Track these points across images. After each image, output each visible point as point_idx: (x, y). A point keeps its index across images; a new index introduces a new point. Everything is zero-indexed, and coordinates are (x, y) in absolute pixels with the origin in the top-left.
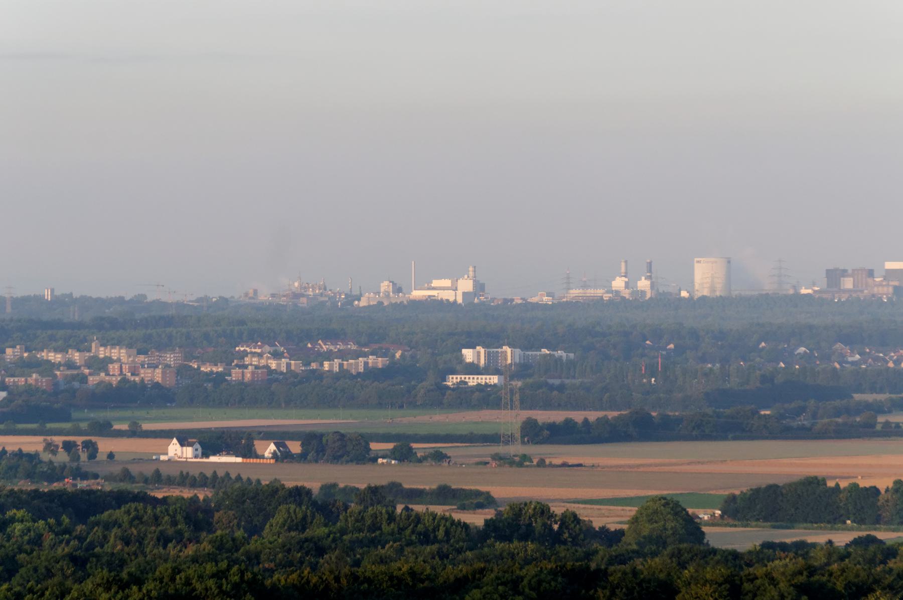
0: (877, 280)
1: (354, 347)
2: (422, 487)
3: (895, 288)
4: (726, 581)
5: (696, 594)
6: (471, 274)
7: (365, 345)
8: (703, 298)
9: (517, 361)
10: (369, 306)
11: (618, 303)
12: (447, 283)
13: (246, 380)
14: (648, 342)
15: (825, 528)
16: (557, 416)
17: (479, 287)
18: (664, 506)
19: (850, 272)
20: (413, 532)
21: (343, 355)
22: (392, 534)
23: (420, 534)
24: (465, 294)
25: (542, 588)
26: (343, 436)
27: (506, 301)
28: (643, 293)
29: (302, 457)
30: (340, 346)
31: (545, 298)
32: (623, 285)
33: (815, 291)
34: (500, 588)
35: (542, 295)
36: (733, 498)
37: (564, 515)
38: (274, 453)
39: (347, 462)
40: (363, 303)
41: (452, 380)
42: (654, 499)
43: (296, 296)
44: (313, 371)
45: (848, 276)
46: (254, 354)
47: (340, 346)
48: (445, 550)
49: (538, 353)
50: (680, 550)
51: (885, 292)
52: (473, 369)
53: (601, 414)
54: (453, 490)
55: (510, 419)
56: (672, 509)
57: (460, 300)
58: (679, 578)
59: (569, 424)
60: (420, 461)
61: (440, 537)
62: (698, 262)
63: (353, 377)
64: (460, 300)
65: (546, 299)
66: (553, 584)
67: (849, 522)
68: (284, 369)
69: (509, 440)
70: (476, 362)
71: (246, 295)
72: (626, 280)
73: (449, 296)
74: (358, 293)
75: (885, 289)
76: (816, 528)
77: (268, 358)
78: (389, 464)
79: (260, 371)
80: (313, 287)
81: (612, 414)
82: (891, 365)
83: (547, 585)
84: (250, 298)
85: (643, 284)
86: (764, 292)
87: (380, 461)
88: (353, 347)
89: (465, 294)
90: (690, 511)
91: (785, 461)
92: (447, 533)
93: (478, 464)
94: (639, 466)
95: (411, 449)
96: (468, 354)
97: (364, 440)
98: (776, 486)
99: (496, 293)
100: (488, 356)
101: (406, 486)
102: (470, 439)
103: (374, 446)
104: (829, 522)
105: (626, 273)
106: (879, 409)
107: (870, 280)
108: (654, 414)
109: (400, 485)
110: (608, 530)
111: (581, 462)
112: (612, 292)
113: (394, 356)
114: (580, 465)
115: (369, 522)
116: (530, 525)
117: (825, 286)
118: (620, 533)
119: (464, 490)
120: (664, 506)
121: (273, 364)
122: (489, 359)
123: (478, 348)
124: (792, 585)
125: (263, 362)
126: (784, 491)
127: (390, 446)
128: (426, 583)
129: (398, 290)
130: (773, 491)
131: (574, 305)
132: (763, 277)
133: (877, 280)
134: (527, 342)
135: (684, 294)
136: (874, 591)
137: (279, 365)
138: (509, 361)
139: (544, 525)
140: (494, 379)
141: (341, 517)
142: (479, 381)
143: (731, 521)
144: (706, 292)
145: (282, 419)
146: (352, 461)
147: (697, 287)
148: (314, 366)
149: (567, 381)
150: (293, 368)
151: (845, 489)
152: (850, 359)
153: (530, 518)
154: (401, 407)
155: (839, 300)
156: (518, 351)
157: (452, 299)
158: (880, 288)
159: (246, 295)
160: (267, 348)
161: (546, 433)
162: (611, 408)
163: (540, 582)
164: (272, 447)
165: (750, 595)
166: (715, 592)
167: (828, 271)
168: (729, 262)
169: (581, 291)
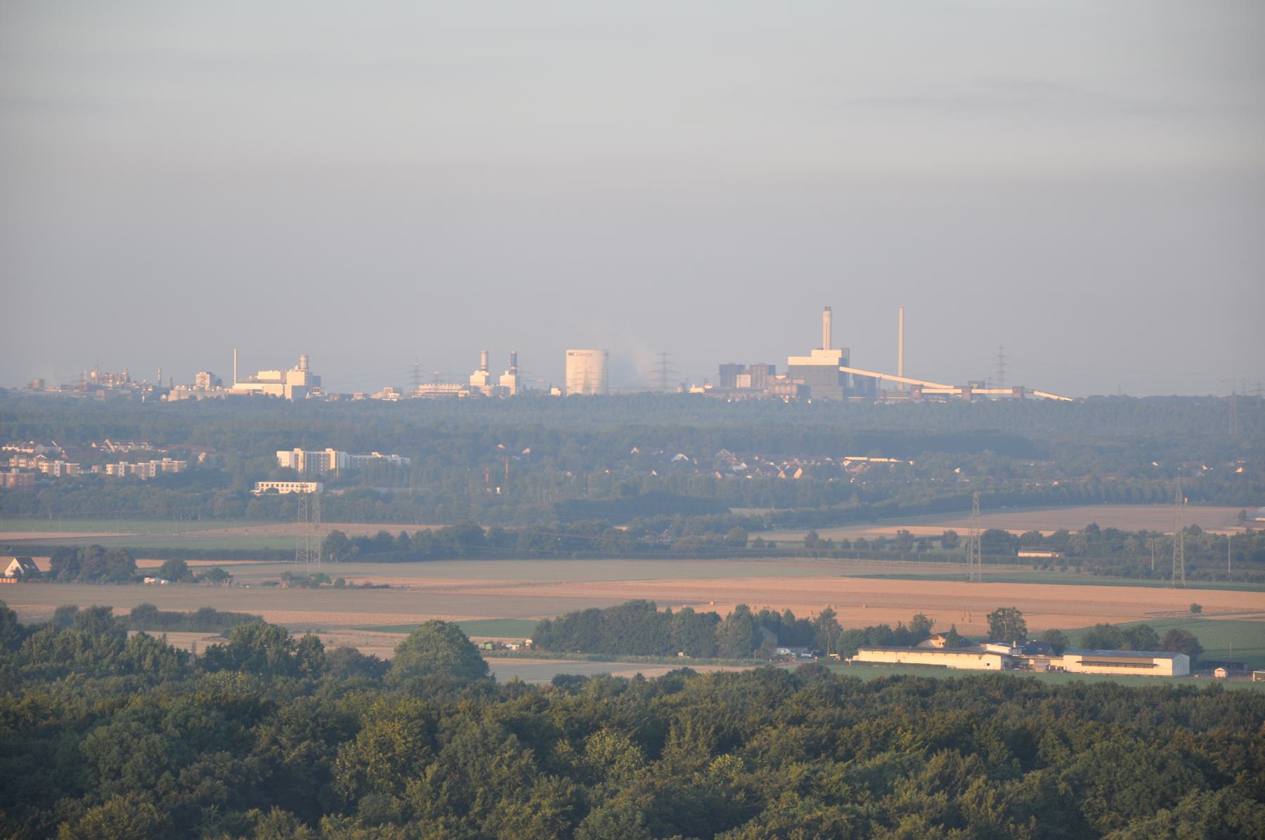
0: (779, 377)
1: (149, 448)
2: (180, 611)
3: (799, 386)
4: (421, 716)
5: (381, 730)
6: (303, 365)
7: (162, 446)
8: (576, 397)
9: (343, 465)
10: (180, 401)
11: (476, 400)
12: (276, 375)
13: (9, 485)
15: (652, 661)
16: (370, 530)
17: (313, 381)
18: (438, 631)
19: (747, 367)
20: (113, 661)
21: (132, 457)
22: (86, 663)
23: (122, 663)
24: (295, 388)
25: (189, 725)
26: (102, 551)
27: (343, 396)
28: (507, 389)
29: (52, 576)
30: (132, 447)
31: (391, 395)
33: (706, 390)
34: (134, 725)
35: (388, 391)
36: (547, 625)
37: (304, 641)
38: (17, 572)
39: (106, 582)
40: (173, 397)
41: (263, 486)
42: (428, 624)
43: (92, 388)
44: (94, 476)
46: (21, 455)
47: (132, 447)
48: (134, 683)
50: (422, 682)
51: (787, 392)
52: (289, 475)
53: (423, 528)
54: (218, 614)
55: (312, 533)
56: (447, 635)
57: (289, 396)
58: (365, 712)
59: (384, 540)
60: (195, 581)
61: (146, 667)
63: (140, 482)
64: (289, 396)
65: (393, 396)
66: (204, 719)
67: (681, 654)
68: (57, 473)
69: (308, 556)
71: (31, 386)
73: (276, 390)
74: (168, 385)
76: (642, 661)
77: (40, 459)
78: (157, 584)
79: (26, 475)
80: (114, 379)
81: (434, 528)
83: (196, 721)
84: (36, 390)
85: (507, 380)
87: (147, 580)
88: (146, 447)
89: (295, 388)
90: (472, 639)
91: (631, 583)
92: (156, 662)
93: (265, 584)
94: (455, 588)
95: (185, 566)
96: (285, 458)
97: (130, 555)
98: (597, 611)
99: (331, 388)
100: (308, 460)
101: (161, 609)
102: (265, 555)
103: (141, 564)
104: (658, 654)
105: (487, 366)
106: (756, 525)
107: (771, 378)
108: (486, 528)
109: (154, 608)
110: (377, 660)
111: (389, 583)
112: (469, 388)
113: (197, 459)
114: (386, 587)
115: (59, 649)
116: (262, 652)
117: (718, 385)
118: (388, 664)
119: (231, 614)
120: (438, 631)
121: (44, 467)
122: (309, 466)
124: (499, 721)
125: (33, 464)
126: (606, 617)
127: (159, 563)
128: (51, 720)
129: (216, 382)
130: (593, 616)
131: (425, 402)
132: (645, 369)
133: (779, 377)
134: (355, 444)
135: (555, 391)
136: (599, 728)
137: (51, 468)
138: (333, 466)
139: (278, 652)
140: (312, 487)
141: (24, 643)
142: (294, 489)
143: (543, 653)
144: (579, 390)
145: (1139, 676)
146: (112, 580)
147: (569, 383)
148: (95, 469)
149: (396, 490)
150: (68, 471)
151: (677, 615)
152: (735, 468)
153: (262, 644)
154: (195, 518)
155: (733, 401)
156: (343, 454)
157: (279, 394)
159: (31, 386)
160: (41, 448)
161: (355, 549)
162: (434, 522)
163: (187, 718)
164: (15, 564)
165: (448, 732)
166: (404, 729)
167: (722, 367)
168: (607, 355)
169: (433, 386)
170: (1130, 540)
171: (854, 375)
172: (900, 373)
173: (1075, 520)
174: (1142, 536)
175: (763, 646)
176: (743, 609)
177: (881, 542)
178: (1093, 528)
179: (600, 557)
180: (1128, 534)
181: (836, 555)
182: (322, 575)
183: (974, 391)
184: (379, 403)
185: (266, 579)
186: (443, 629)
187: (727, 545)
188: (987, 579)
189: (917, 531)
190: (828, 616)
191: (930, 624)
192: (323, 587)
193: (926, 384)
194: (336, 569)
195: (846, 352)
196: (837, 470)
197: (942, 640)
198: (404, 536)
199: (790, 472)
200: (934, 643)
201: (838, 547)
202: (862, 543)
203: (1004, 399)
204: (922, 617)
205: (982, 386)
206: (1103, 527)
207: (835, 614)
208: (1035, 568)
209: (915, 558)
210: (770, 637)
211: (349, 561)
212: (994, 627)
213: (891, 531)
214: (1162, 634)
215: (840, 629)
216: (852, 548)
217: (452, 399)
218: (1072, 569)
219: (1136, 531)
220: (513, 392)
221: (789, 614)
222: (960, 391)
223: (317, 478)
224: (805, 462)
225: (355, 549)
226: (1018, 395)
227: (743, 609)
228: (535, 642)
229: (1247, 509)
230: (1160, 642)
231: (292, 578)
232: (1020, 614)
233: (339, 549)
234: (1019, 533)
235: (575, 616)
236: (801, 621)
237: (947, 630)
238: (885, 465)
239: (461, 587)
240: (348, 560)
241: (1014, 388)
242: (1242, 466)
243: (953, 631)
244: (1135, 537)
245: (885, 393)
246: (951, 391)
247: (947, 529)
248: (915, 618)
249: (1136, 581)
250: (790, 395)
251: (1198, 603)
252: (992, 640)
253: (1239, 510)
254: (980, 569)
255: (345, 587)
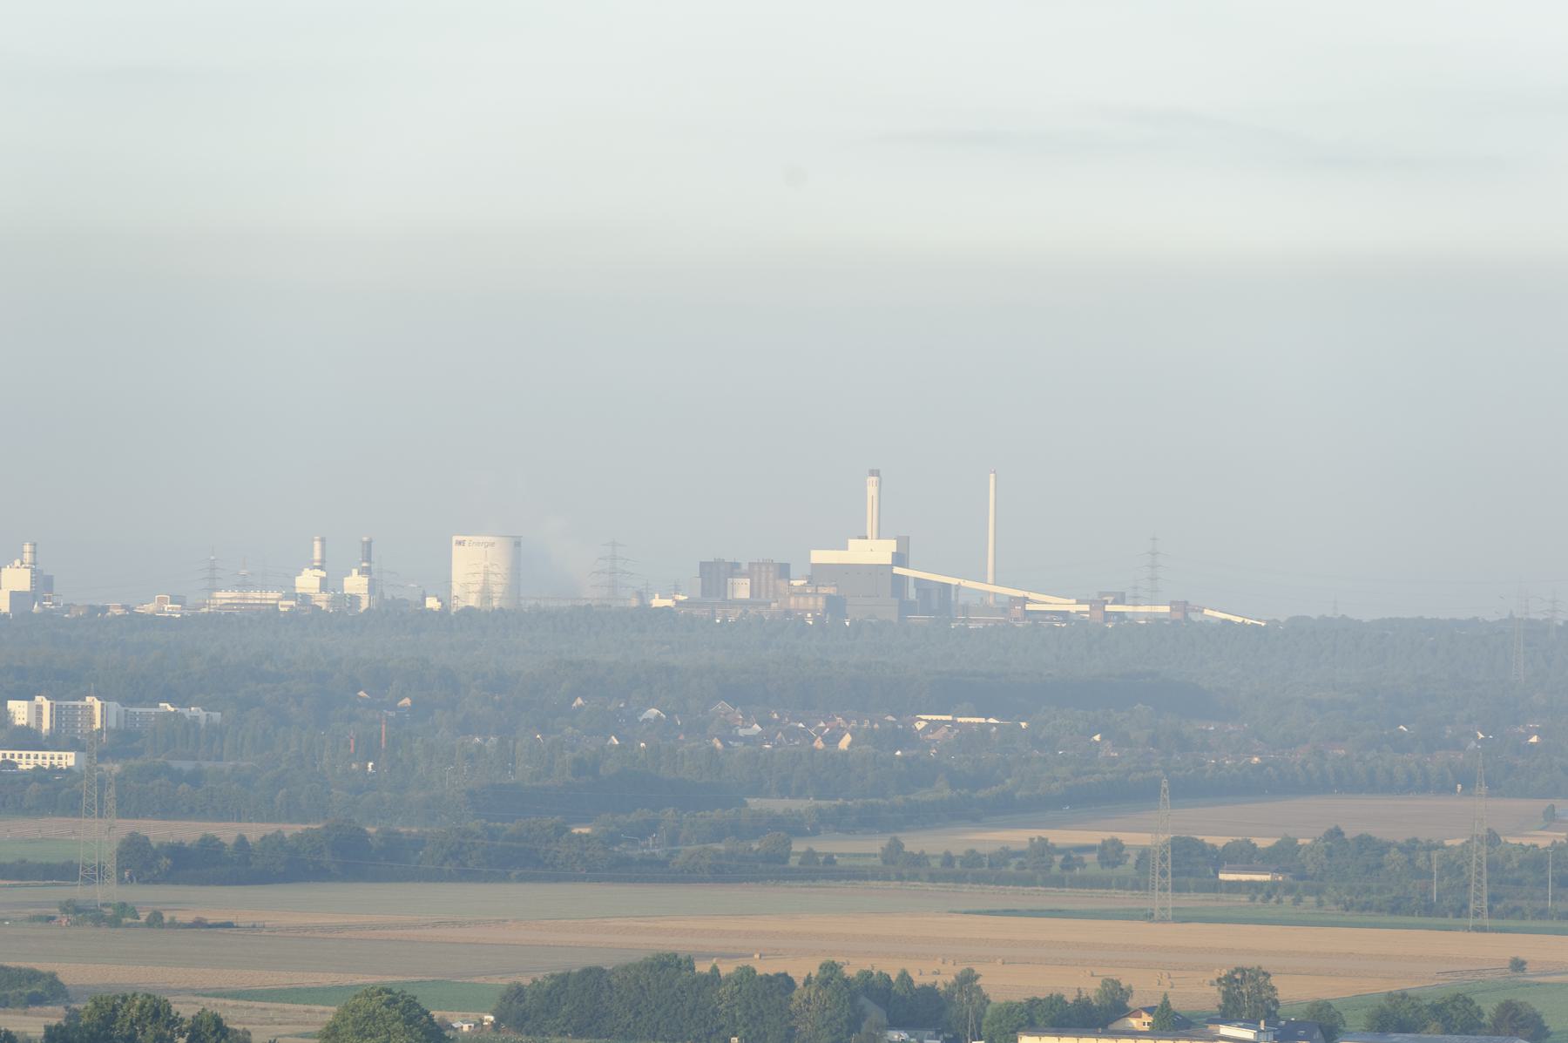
0: (796, 583)
3: (828, 598)
6: (27, 557)
8: (468, 611)
9: (113, 724)
11: (305, 616)
14: (362, 693)
16: (188, 832)
17: (43, 583)
19: (745, 567)
27: (93, 610)
28: (355, 599)
32: (317, 583)
33: (678, 603)
35: (162, 601)
36: (518, 992)
37: (197, 1021)
42: (369, 993)
45: (743, 575)
49: (153, 710)
51: (810, 606)
52: (28, 739)
53: (270, 828)
55: (96, 836)
62: (459, 543)
69: (94, 874)
70: (33, 725)
72: (323, 574)
75: (811, 601)
81: (291, 829)
82: (819, 744)
85: (355, 584)
86: (583, 603)
90: (437, 1015)
93: (33, 919)
96: (19, 711)
100: (57, 713)
105: (323, 561)
106: (794, 827)
107: (782, 584)
108: (371, 830)
111: (231, 919)
112: (294, 596)
114: (229, 925)
117: (698, 594)
120: (387, 1005)
122: (59, 724)
123: (38, 698)
126: (615, 981)
131: (223, 620)
133: (796, 583)
135: (432, 603)
140: (68, 759)
142: (40, 761)
144: (473, 601)
147: (456, 590)
149: (206, 765)
151: (729, 978)
152: (742, 732)
153: (132, 1024)
155: (724, 620)
156: (114, 706)
158: (801, 600)
167: (703, 565)
168: (518, 544)
169: (236, 594)
170: (1393, 853)
171: (916, 579)
172: (990, 578)
173: (1304, 820)
174: (1411, 847)
175: (865, 1027)
176: (831, 968)
177: (1005, 855)
178: (1336, 834)
179: (558, 879)
180: (1390, 845)
181: (933, 878)
182: (124, 905)
183: (1109, 608)
184: (151, 621)
185: (33, 911)
186: (395, 1001)
187: (762, 861)
188: (1182, 917)
189: (1061, 837)
190: (967, 980)
191: (1128, 993)
192: (128, 926)
193: (1032, 596)
194: (145, 896)
195: (903, 542)
196: (907, 737)
197: (1147, 1018)
198: (242, 842)
199: (833, 739)
200: (1134, 1023)
201: (936, 864)
202: (973, 859)
203: (1157, 621)
204: (1117, 983)
205: (1120, 599)
206: (1350, 833)
207: (977, 977)
208: (1253, 899)
209: (1059, 882)
210: (875, 1014)
211: (156, 882)
212: (1227, 997)
213: (1018, 837)
214: (1489, 1007)
215: (986, 1001)
216: (957, 865)
217: (269, 615)
218: (1310, 900)
219: (1401, 840)
220: (364, 605)
221: (905, 977)
222: (1086, 608)
223: (73, 745)
224: (854, 723)
225: (165, 862)
226: (1178, 615)
227: (831, 968)
228: (500, 1019)
229: (1557, 802)
230: (1486, 1019)
231: (77, 910)
232: (1267, 975)
233: (141, 862)
234: (1220, 841)
235: (564, 979)
236: (924, 987)
237: (1157, 1002)
238: (984, 728)
239: (346, 927)
240: (154, 881)
241: (1171, 604)
242: (1538, 732)
243: (1166, 1004)
244: (1401, 848)
245: (966, 609)
246: (1071, 606)
247: (1107, 836)
248: (1104, 984)
249: (1410, 920)
250: (813, 612)
251: (1522, 956)
252: (1227, 1019)
253: (1545, 804)
254: (1170, 900)
255: (162, 926)
